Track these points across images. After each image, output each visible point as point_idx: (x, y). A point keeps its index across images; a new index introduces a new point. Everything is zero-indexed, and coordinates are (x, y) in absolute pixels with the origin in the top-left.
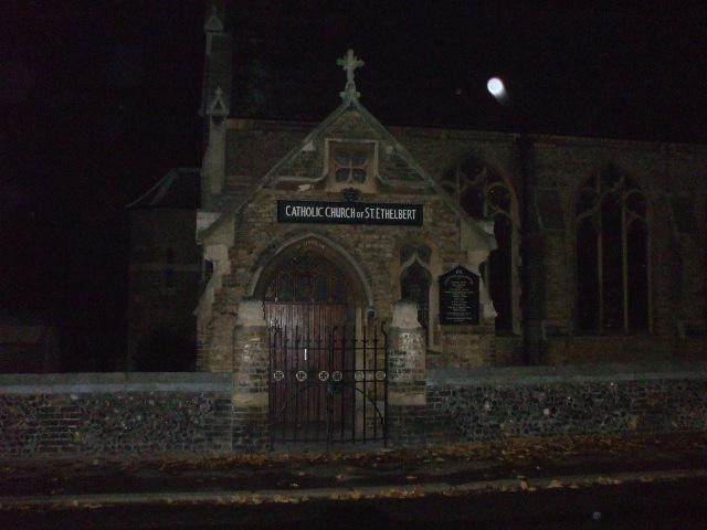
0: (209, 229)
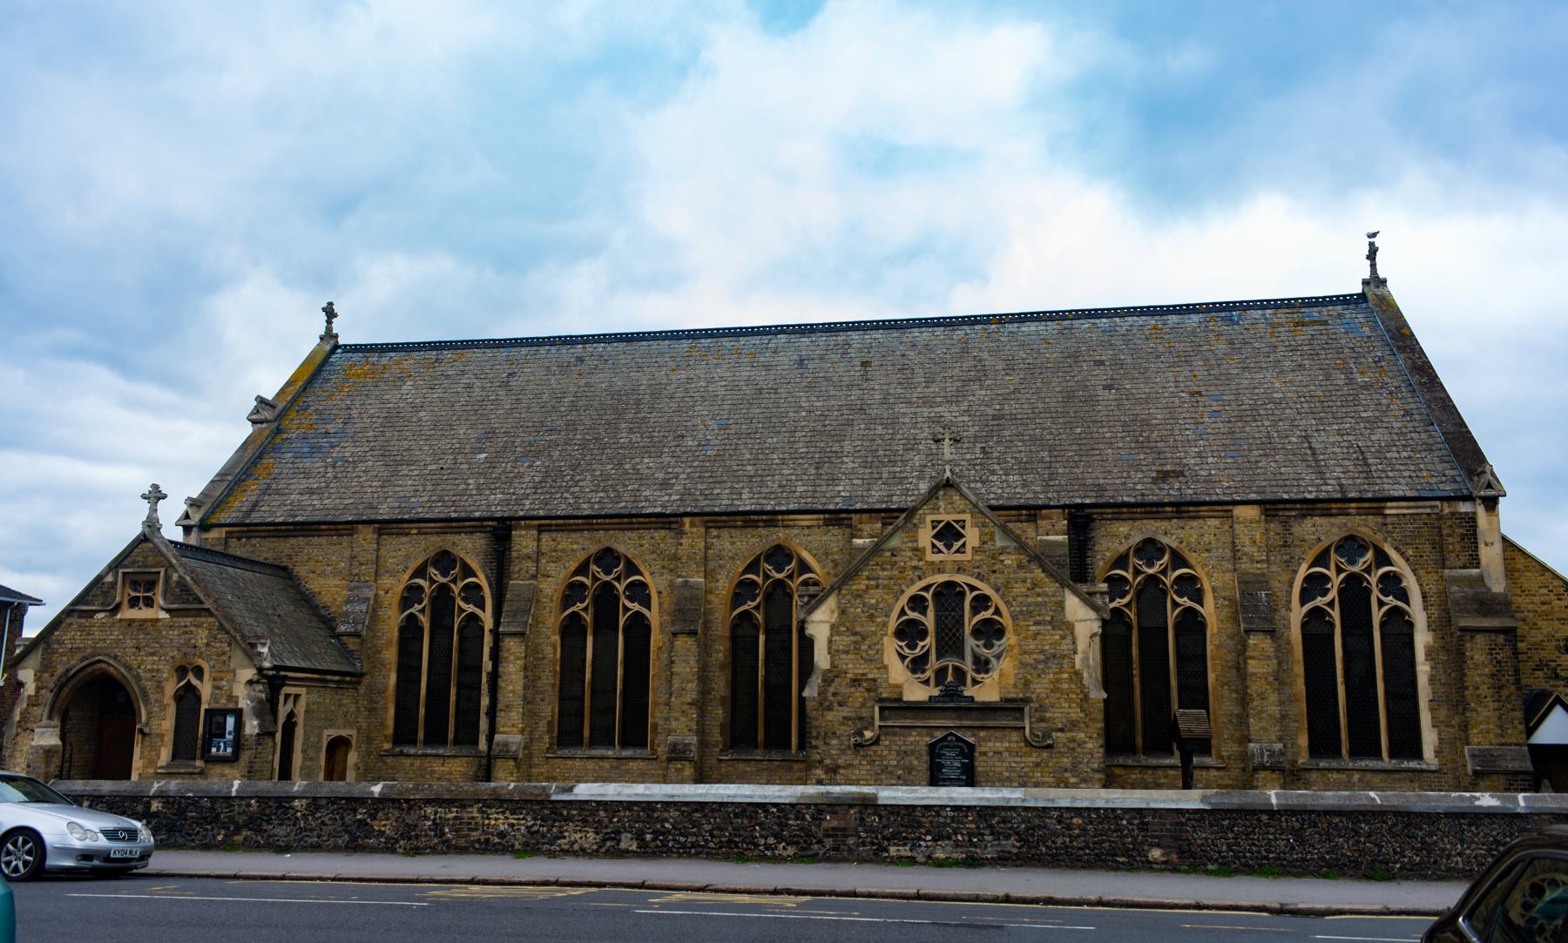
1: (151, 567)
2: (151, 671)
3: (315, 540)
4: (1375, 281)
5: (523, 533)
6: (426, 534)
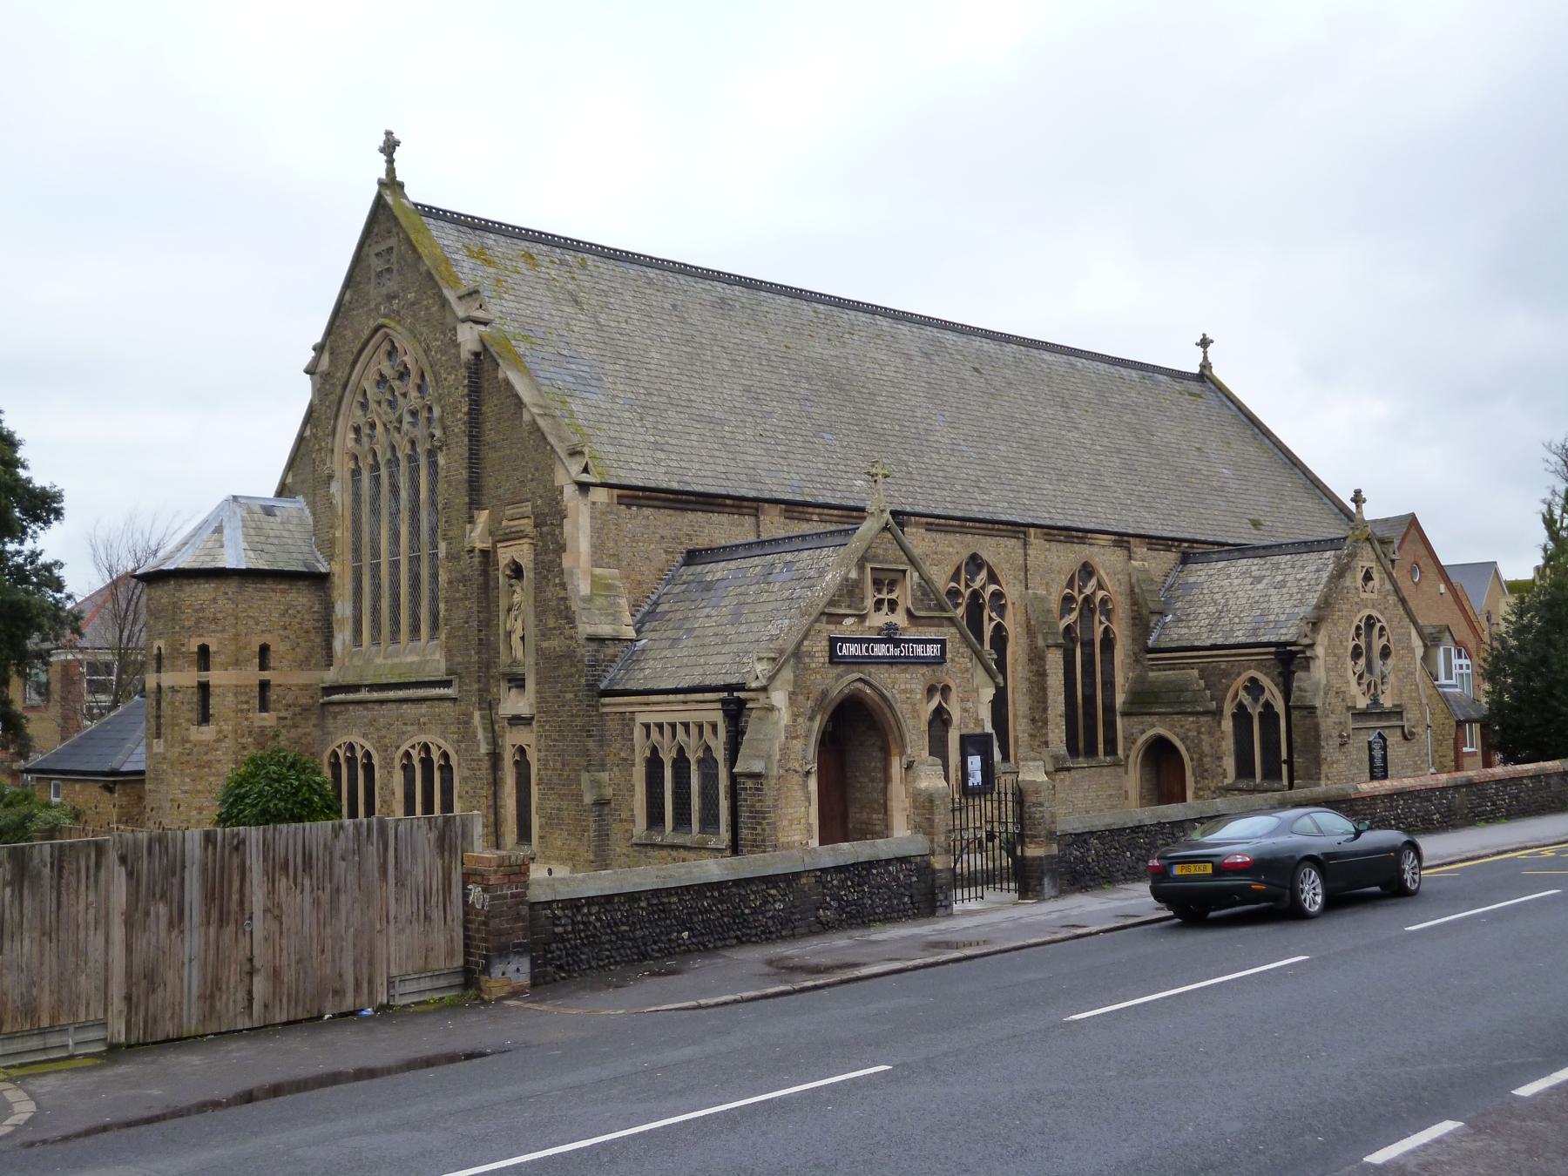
0: (1490, 758)
1: (891, 563)
2: (905, 691)
3: (715, 517)
4: (1206, 365)
5: (914, 530)
6: (826, 522)
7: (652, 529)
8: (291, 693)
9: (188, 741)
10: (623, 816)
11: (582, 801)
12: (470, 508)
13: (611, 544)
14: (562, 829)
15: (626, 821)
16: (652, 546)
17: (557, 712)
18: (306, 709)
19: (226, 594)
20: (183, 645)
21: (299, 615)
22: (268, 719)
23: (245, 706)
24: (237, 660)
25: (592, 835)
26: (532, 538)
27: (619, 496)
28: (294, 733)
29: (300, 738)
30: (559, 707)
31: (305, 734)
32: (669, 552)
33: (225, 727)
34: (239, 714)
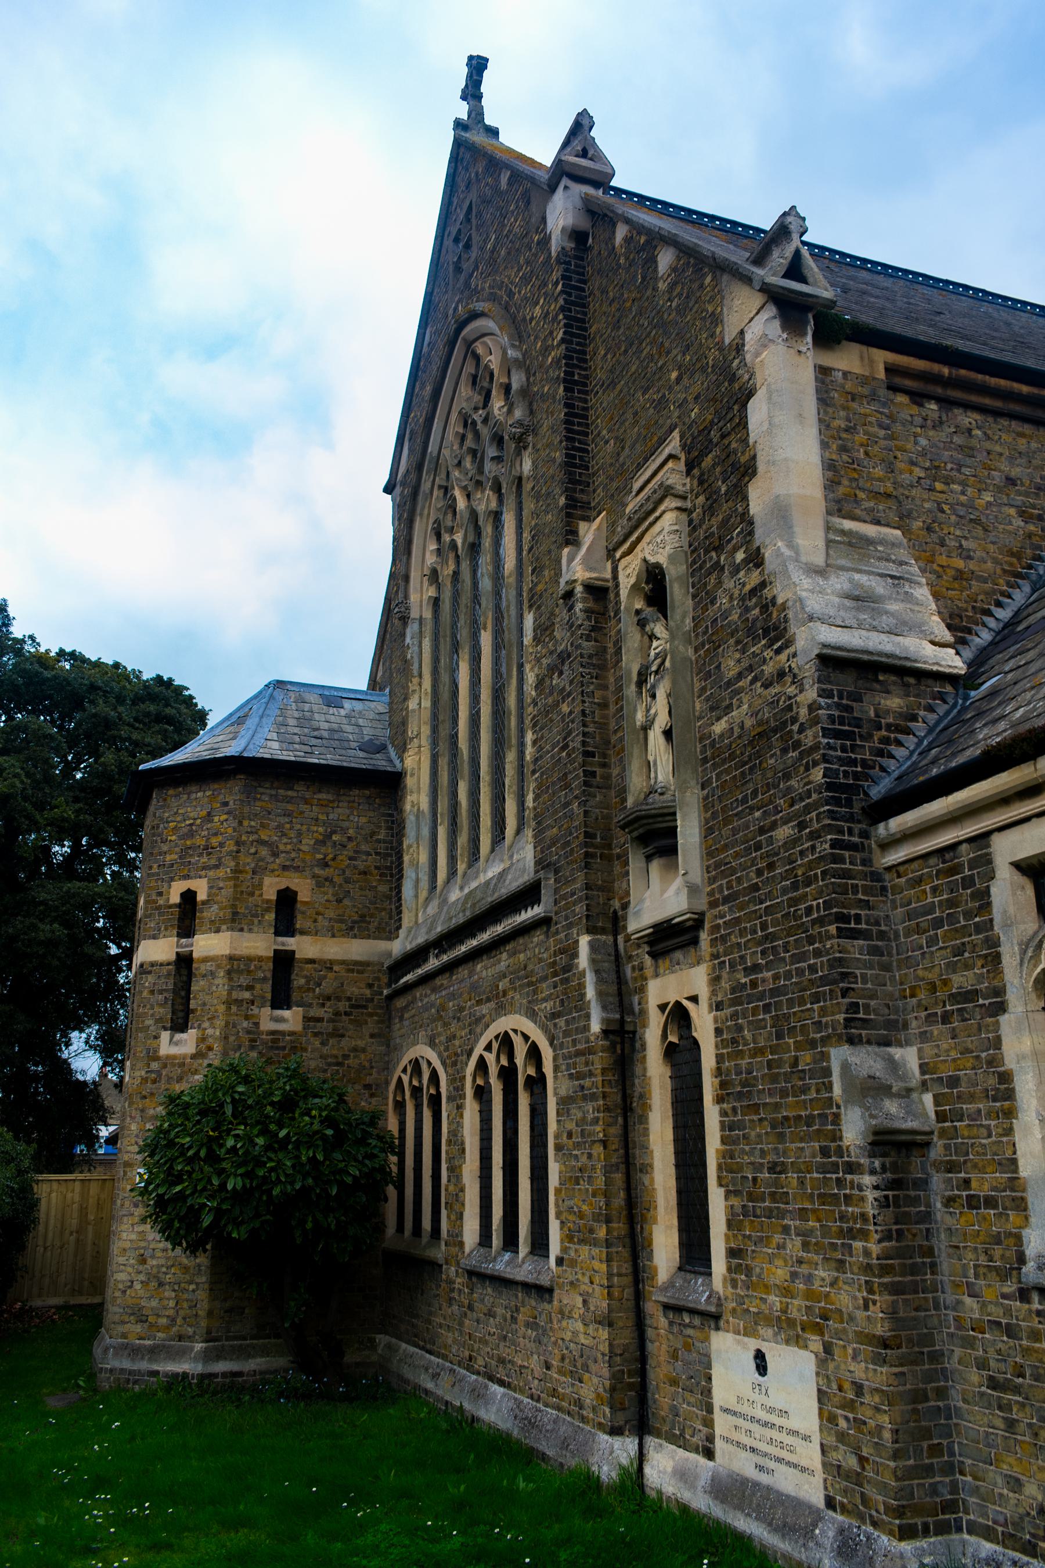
7: (981, 457)
8: (330, 975)
9: (157, 1058)
10: (981, 1186)
11: (836, 1136)
12: (568, 515)
13: (878, 472)
14: (786, 1230)
15: (990, 1202)
16: (988, 497)
17: (755, 888)
18: (358, 1005)
19: (226, 804)
20: (160, 894)
21: (350, 845)
22: (291, 1019)
23: (247, 995)
24: (235, 914)
25: (875, 1248)
26: (684, 498)
27: (890, 370)
28: (332, 1048)
29: (346, 1057)
30: (759, 873)
31: (355, 1049)
32: (1031, 516)
33: (210, 1031)
34: (234, 1008)
